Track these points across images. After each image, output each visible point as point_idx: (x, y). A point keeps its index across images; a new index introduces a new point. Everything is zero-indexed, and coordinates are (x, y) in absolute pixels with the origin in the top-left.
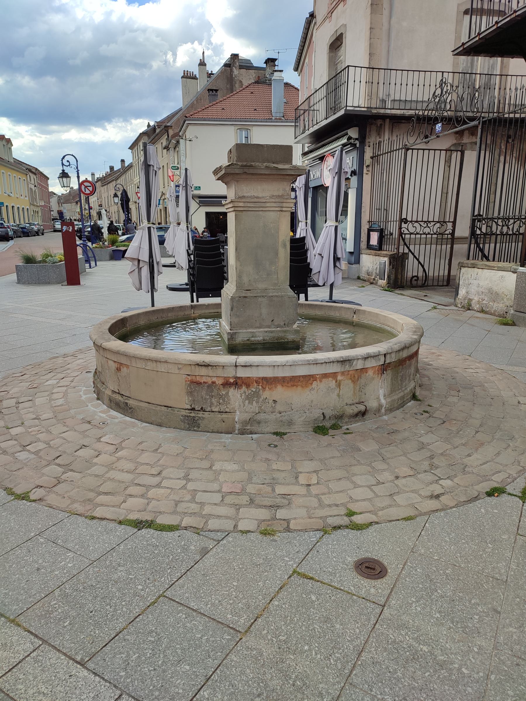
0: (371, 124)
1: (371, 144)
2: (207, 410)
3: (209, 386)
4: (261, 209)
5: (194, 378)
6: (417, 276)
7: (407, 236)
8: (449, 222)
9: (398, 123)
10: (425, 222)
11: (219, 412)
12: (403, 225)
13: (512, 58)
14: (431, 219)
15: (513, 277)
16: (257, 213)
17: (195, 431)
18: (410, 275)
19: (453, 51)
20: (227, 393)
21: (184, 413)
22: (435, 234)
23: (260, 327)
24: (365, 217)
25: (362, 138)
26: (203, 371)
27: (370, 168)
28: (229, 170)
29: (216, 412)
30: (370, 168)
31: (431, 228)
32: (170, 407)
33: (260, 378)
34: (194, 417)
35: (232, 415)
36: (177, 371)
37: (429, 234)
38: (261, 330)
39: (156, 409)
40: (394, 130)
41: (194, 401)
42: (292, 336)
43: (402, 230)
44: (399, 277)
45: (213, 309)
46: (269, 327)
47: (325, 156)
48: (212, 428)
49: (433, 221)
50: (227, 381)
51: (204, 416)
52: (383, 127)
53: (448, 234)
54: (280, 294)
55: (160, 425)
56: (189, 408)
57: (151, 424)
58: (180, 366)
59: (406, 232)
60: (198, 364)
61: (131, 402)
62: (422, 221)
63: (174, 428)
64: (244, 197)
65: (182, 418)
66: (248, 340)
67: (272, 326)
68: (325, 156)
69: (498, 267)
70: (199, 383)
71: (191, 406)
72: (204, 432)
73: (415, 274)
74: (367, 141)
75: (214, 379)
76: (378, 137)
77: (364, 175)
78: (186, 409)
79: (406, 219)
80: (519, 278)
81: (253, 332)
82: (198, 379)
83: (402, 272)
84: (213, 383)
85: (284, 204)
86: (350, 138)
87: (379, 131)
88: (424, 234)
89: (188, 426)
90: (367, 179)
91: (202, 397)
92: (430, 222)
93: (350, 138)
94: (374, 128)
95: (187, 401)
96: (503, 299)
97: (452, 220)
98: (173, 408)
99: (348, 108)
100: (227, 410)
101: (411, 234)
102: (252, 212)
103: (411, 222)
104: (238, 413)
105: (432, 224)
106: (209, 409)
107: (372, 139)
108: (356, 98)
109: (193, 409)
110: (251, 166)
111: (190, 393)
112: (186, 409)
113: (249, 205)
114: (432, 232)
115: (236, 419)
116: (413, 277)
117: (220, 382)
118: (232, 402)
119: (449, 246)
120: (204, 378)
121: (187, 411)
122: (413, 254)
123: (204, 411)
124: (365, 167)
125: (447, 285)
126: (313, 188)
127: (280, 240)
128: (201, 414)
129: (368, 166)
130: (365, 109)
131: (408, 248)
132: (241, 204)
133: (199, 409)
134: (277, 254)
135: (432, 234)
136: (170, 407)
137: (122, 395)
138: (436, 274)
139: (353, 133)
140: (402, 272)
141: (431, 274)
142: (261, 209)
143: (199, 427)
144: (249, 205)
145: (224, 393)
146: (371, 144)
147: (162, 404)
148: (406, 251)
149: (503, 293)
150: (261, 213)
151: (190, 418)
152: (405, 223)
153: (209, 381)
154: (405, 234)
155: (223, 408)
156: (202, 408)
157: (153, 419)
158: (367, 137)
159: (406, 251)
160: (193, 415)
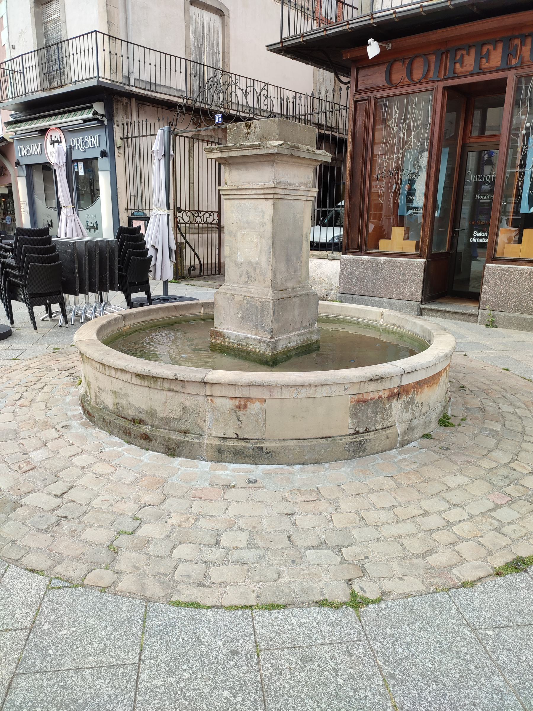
0: (118, 101)
1: (120, 124)
2: (371, 430)
3: (376, 403)
4: (293, 197)
5: (361, 396)
6: (194, 267)
7: (183, 225)
8: (215, 212)
9: (143, 104)
10: (197, 211)
11: (382, 429)
12: (179, 215)
13: (307, 64)
14: (201, 209)
15: (336, 264)
16: (289, 201)
17: (360, 457)
18: (188, 264)
19: (267, 46)
20: (390, 406)
21: (348, 440)
22: (205, 223)
23: (292, 332)
24: (122, 205)
25: (110, 114)
26: (373, 386)
27: (122, 150)
28: (280, 149)
29: (379, 429)
30: (122, 150)
31: (202, 217)
32: (330, 437)
33: (415, 382)
34: (360, 441)
35: (393, 428)
36: (342, 393)
37: (200, 223)
38: (294, 334)
39: (312, 443)
40: (140, 112)
41: (358, 423)
42: (316, 337)
43: (178, 219)
44: (179, 268)
45: (141, 317)
46: (299, 329)
47: (49, 128)
48: (377, 448)
49: (203, 211)
50: (392, 393)
51: (370, 437)
52: (129, 106)
53: (215, 224)
54: (305, 292)
55: (317, 462)
56: (352, 431)
57: (303, 464)
58: (347, 386)
59: (182, 221)
60: (371, 380)
61: (267, 445)
62: (194, 211)
63: (336, 461)
64: (280, 182)
65: (347, 446)
66: (286, 347)
67: (302, 328)
68: (49, 128)
69: (313, 255)
70: (365, 402)
71: (355, 429)
72: (369, 455)
73: (193, 264)
74: (115, 119)
75: (381, 393)
76: (125, 117)
77: (116, 157)
78: (349, 435)
79: (180, 208)
80: (343, 265)
81: (290, 338)
82: (366, 397)
83: (181, 263)
84: (380, 397)
85: (310, 193)
86: (95, 113)
87: (126, 110)
88: (197, 223)
89: (352, 454)
90: (119, 161)
91: (367, 417)
92: (200, 211)
93: (95, 113)
94: (120, 106)
95: (350, 425)
96: (321, 284)
97: (217, 210)
98: (333, 437)
99: (100, 79)
100: (389, 425)
101: (186, 223)
102: (236, 201)
103: (185, 211)
104: (397, 425)
105: (203, 213)
106: (373, 428)
107: (120, 118)
108: (83, 69)
109: (357, 433)
110: (297, 148)
111: (355, 415)
112: (349, 435)
113: (287, 192)
114: (202, 222)
115: (399, 432)
116: (191, 266)
117: (385, 395)
118: (393, 415)
119: (217, 235)
120: (371, 394)
121: (351, 437)
122: (189, 244)
123: (368, 432)
124: (116, 149)
125: (219, 274)
126: (27, 166)
127: (304, 233)
128: (366, 436)
129: (119, 148)
130: (109, 82)
131: (185, 238)
132: (280, 191)
133: (363, 431)
134: (301, 248)
135: (203, 224)
136: (330, 437)
137: (246, 439)
138: (210, 262)
139: (99, 108)
140: (181, 263)
141: (205, 262)
142: (293, 197)
143: (364, 452)
144: (287, 192)
145: (388, 406)
146: (120, 124)
147: (318, 436)
148: (183, 241)
149: (320, 278)
150: (292, 202)
151: (356, 444)
152: (180, 212)
153: (376, 395)
154: (181, 223)
155: (386, 423)
156: (366, 430)
157: (306, 458)
158: (115, 115)
159: (183, 241)
160: (358, 439)
